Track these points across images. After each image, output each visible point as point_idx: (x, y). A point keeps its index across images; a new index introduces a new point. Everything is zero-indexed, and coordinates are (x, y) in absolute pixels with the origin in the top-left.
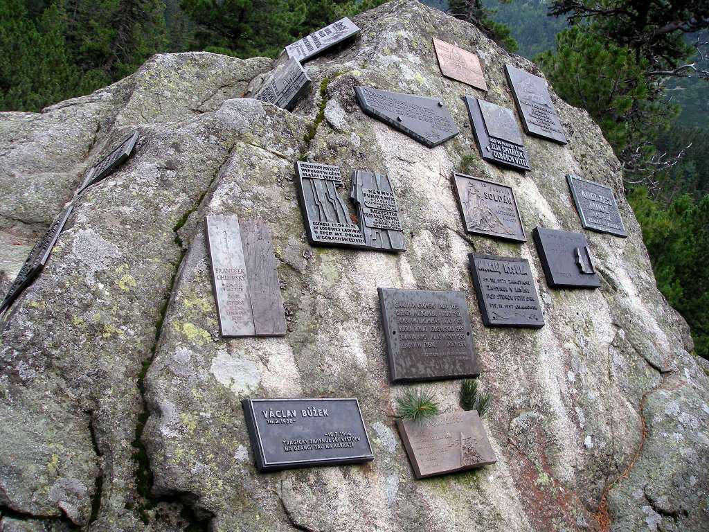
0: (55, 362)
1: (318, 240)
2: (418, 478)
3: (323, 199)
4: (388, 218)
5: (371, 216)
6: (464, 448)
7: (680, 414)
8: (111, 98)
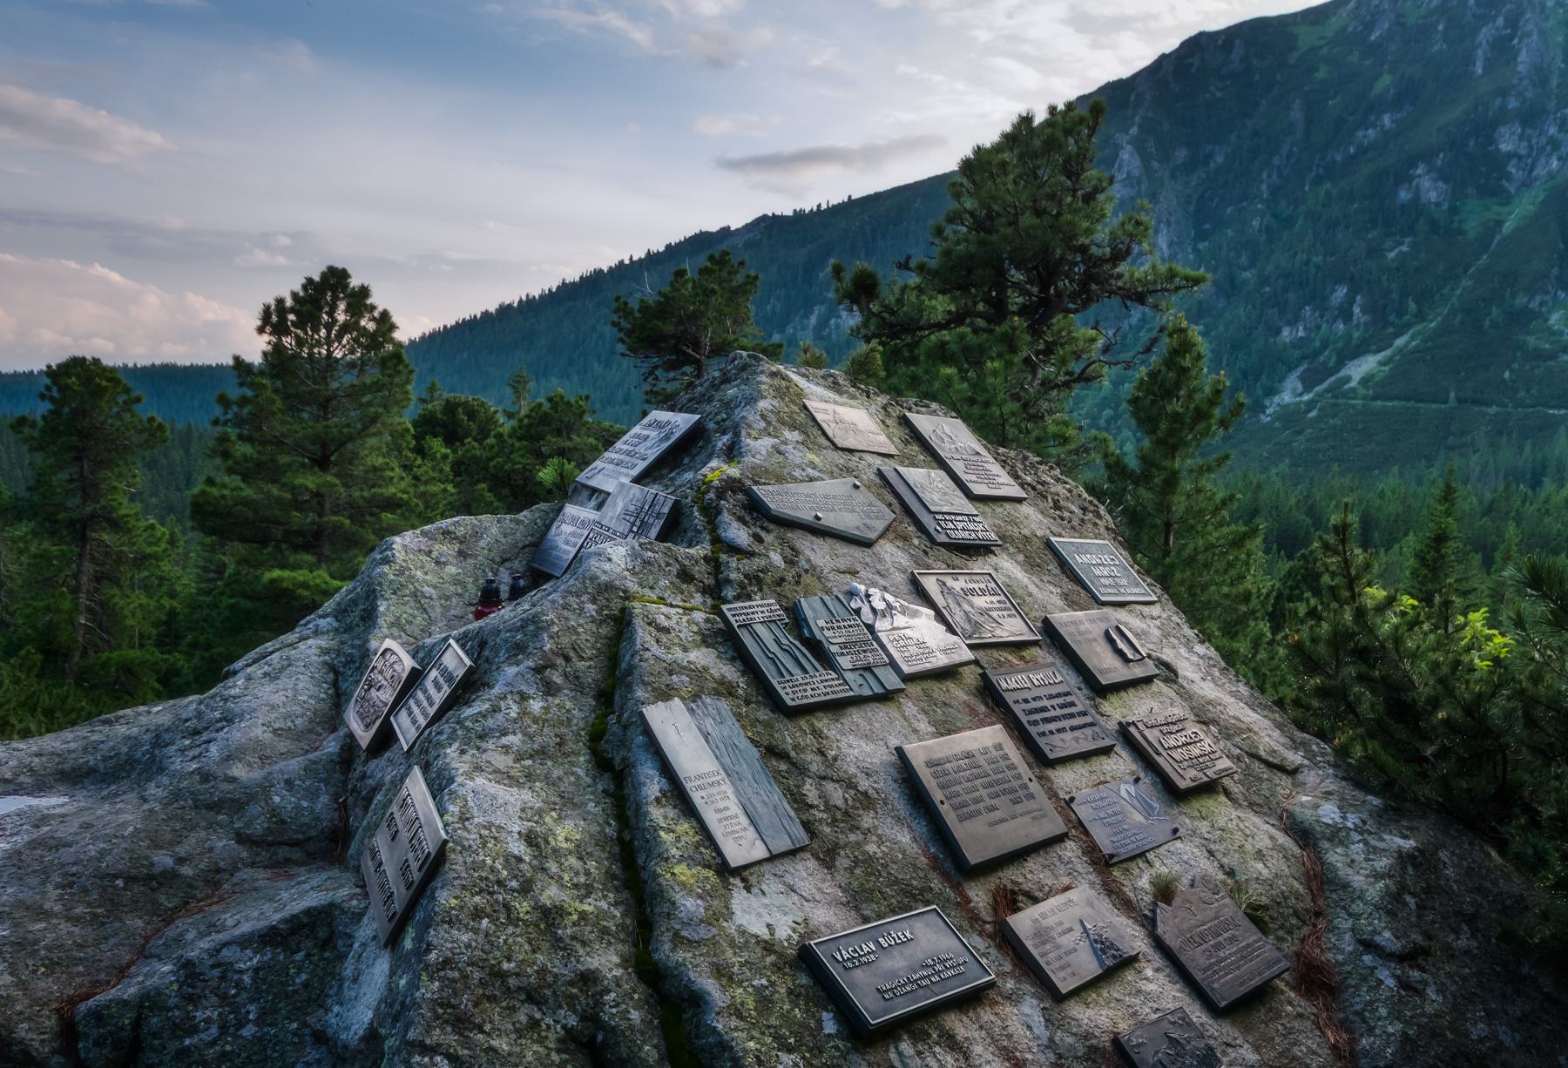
0: (512, 982)
1: (794, 703)
2: (1057, 997)
3: (774, 647)
4: (865, 651)
5: (842, 654)
6: (1096, 941)
7: (1344, 818)
8: (336, 624)
